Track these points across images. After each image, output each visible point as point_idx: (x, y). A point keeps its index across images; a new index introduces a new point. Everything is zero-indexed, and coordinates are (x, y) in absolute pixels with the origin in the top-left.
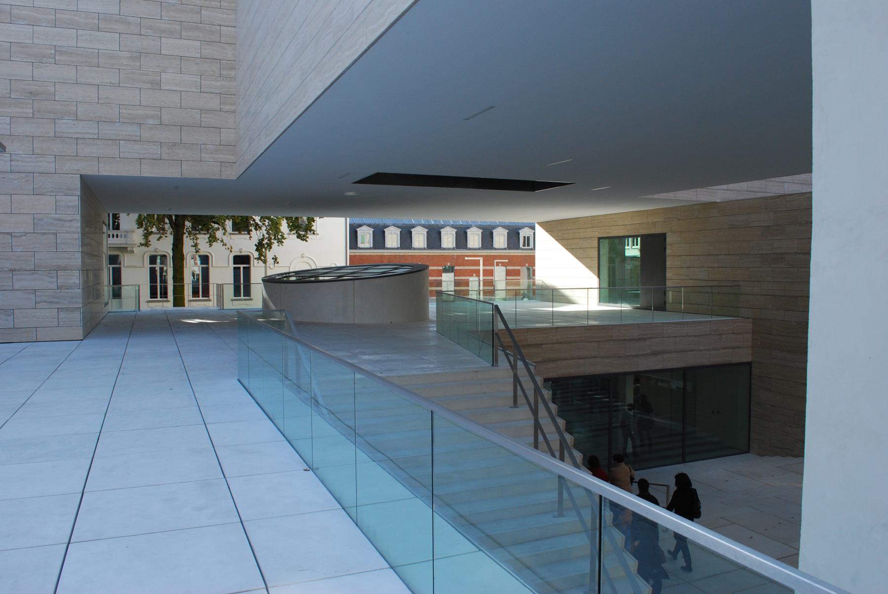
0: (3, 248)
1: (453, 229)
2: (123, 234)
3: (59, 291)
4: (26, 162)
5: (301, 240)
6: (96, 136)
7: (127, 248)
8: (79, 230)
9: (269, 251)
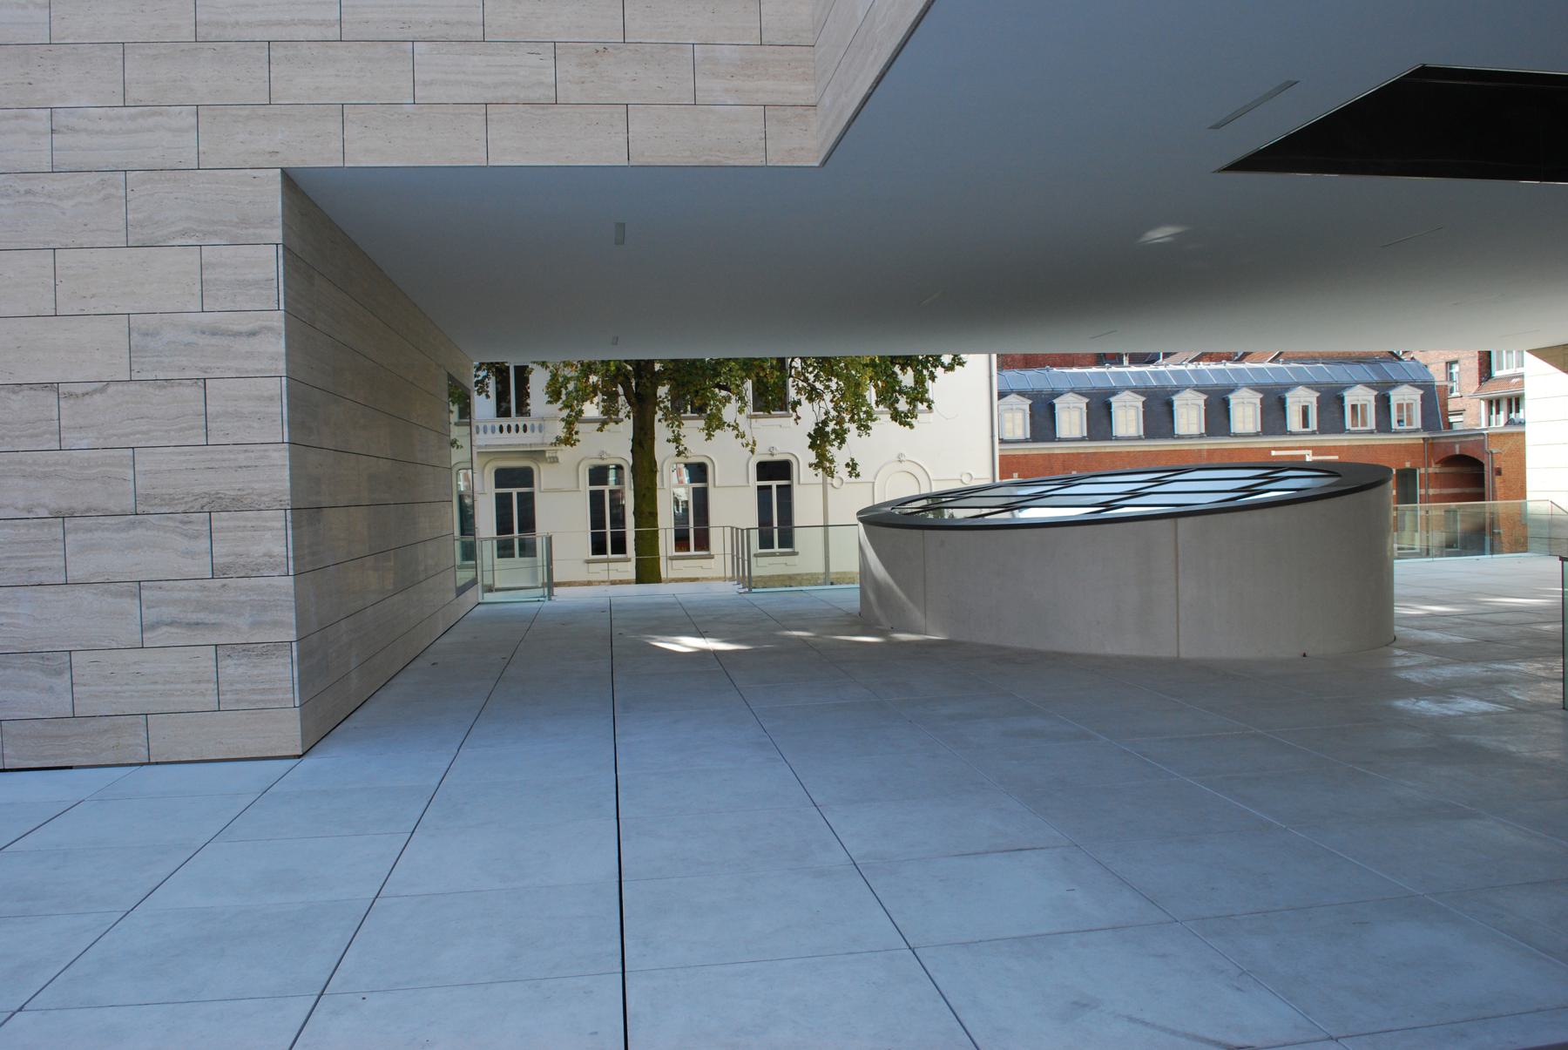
0: (32, 436)
1: (1199, 394)
2: (536, 424)
3: (218, 583)
4: (101, 132)
5: (901, 423)
6: (333, 33)
7: (544, 452)
8: (281, 366)
9: (840, 448)
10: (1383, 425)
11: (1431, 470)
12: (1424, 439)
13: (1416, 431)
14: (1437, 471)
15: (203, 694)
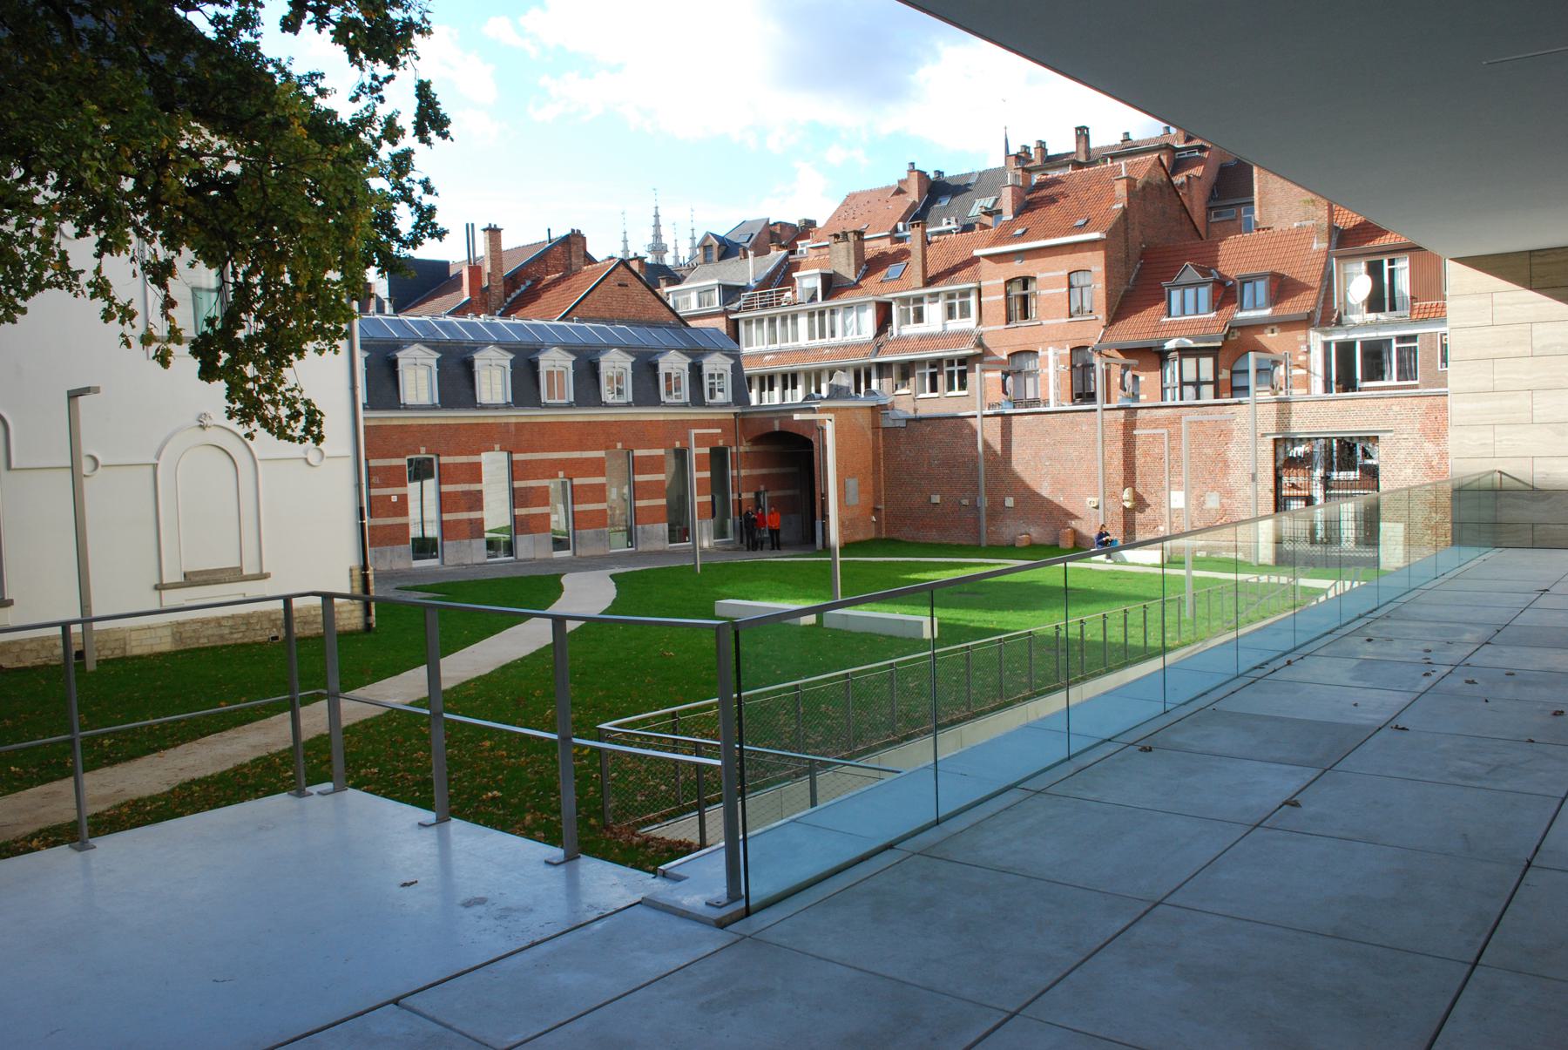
1: (505, 353)
10: (697, 399)
11: (742, 449)
12: (735, 414)
13: (727, 405)
14: (748, 449)
15: (1294, 486)
